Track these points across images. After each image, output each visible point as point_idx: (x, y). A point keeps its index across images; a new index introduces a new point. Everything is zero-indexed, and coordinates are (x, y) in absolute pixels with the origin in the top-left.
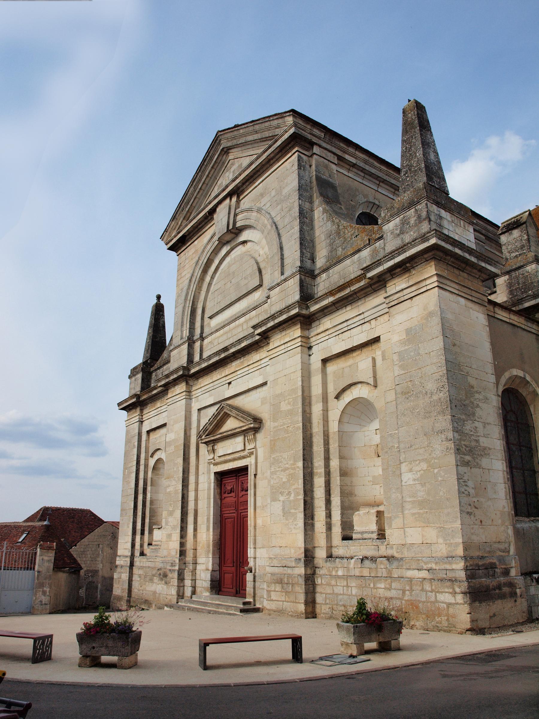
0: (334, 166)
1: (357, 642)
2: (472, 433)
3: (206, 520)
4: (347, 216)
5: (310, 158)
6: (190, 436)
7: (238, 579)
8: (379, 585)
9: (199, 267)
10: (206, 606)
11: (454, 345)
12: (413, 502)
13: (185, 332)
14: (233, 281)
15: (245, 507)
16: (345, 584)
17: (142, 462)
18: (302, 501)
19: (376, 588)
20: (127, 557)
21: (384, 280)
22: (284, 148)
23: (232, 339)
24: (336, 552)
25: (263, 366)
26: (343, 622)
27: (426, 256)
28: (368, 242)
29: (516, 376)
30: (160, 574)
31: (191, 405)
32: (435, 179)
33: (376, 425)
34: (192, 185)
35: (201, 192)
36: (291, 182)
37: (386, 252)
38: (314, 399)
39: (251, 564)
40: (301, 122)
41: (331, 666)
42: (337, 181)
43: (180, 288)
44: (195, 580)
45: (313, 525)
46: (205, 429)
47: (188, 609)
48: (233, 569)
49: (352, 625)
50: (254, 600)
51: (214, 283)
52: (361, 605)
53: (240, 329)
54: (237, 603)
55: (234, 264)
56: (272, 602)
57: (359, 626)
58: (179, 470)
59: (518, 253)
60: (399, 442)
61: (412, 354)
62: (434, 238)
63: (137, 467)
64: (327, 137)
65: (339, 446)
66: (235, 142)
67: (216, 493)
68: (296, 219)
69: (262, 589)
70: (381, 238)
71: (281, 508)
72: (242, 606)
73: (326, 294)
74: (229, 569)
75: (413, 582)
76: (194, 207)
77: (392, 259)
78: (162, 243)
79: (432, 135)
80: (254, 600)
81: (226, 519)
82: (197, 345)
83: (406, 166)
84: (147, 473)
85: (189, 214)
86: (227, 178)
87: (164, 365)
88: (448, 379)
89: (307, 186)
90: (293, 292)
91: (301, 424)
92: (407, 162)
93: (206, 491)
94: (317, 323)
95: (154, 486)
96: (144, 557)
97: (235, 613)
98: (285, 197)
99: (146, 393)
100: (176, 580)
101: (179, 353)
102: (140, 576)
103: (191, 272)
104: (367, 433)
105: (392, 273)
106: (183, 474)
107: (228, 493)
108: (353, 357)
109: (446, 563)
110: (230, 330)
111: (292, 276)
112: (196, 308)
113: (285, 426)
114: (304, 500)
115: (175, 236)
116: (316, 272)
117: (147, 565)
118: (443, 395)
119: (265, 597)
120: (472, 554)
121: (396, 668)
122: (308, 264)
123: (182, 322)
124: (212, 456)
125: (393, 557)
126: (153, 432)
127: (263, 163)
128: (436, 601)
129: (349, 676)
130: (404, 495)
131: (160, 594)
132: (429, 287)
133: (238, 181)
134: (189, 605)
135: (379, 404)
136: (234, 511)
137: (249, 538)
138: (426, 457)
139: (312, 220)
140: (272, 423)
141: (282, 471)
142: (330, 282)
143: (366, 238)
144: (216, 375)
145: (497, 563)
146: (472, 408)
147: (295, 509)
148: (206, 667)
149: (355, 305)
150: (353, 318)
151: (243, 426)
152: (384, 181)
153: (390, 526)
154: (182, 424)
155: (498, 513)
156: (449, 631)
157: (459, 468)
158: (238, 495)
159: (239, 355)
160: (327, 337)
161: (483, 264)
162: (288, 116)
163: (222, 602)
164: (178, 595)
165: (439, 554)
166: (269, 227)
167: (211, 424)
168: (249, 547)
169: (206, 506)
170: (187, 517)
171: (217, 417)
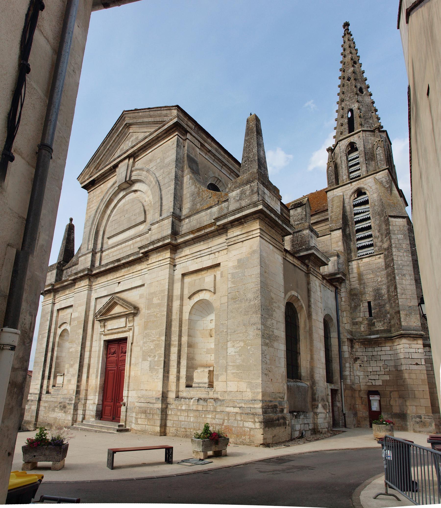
0: (198, 149)
1: (204, 451)
2: (270, 326)
3: (95, 372)
4: (204, 184)
5: (184, 141)
6: (89, 315)
7: (115, 410)
8: (208, 416)
9: (103, 203)
10: (93, 427)
11: (265, 272)
12: (233, 366)
13: (90, 245)
14: (126, 216)
15: (123, 364)
16: (187, 414)
17: (53, 330)
18: (163, 362)
19: (206, 418)
20: (36, 394)
21: (226, 228)
22: (168, 131)
23: (122, 254)
24: (181, 394)
25: (143, 274)
26: (196, 438)
27: (254, 216)
28: (217, 202)
29: (294, 295)
30: (61, 406)
31: (91, 294)
32: (262, 168)
33: (212, 316)
34: (102, 145)
35: (108, 151)
36: (171, 155)
37: (230, 210)
38: (175, 298)
39: (125, 400)
40: (181, 115)
41: (191, 466)
42: (199, 159)
43: (89, 215)
44: (85, 410)
45: (168, 377)
46: (100, 312)
47: (80, 430)
48: (112, 403)
49: (202, 440)
50: (126, 424)
51: (112, 216)
52: (207, 428)
53: (128, 248)
54: (114, 426)
55: (127, 204)
56: (138, 425)
57: (206, 441)
58: (79, 338)
59: (299, 222)
60: (227, 329)
61: (240, 275)
62: (262, 205)
63: (48, 334)
64: (196, 129)
65: (188, 329)
66: (135, 121)
67: (104, 354)
68: (172, 180)
69: (131, 416)
70: (227, 200)
71: (149, 365)
72: (118, 428)
73: (189, 232)
74: (109, 403)
75: (230, 415)
76: (103, 161)
77: (233, 215)
78: (78, 183)
79: (263, 140)
80: (126, 424)
81: (109, 371)
82: (98, 255)
83: (246, 157)
84: (55, 338)
85: (98, 166)
86: (127, 145)
87: (73, 266)
88: (261, 292)
89: (181, 159)
90: (167, 228)
91: (166, 313)
92: (247, 154)
93: (97, 352)
94: (181, 250)
95: (59, 347)
96: (49, 394)
97: (113, 432)
98: (167, 164)
99: (59, 284)
100: (72, 410)
101: (85, 259)
102: (45, 407)
103: (98, 205)
104: (205, 322)
105: (232, 224)
106: (82, 340)
107: (112, 354)
108: (202, 274)
109: (251, 404)
110: (121, 248)
111: (167, 218)
112: (99, 230)
113: (155, 313)
114: (164, 361)
115: (88, 179)
116: (182, 218)
117: (51, 400)
118: (257, 302)
119: (134, 422)
120: (266, 399)
121: (229, 467)
122: (178, 211)
123: (89, 239)
124: (103, 330)
125: (218, 399)
126: (62, 310)
127: (154, 139)
128: (243, 427)
129: (205, 472)
130: (228, 361)
131: (59, 419)
132: (254, 236)
133: (135, 148)
134: (81, 426)
135: (216, 304)
136: (115, 366)
137: (124, 384)
138: (243, 339)
139: (182, 183)
140: (146, 311)
141: (151, 341)
142: (190, 225)
143: (216, 200)
144: (110, 277)
145: (278, 405)
146: (271, 311)
147: (158, 366)
148: (113, 468)
149: (206, 242)
150: (204, 250)
151: (126, 311)
152: (225, 165)
153: (217, 380)
154: (84, 307)
155: (280, 375)
156: (250, 445)
157: (263, 346)
158: (119, 356)
159: (127, 265)
160: (186, 260)
161: (285, 226)
162: (174, 109)
163: (104, 425)
164: (73, 420)
165: (247, 398)
166: (154, 183)
167: (104, 308)
168: (124, 389)
169: (96, 362)
170: (82, 369)
171: (109, 304)
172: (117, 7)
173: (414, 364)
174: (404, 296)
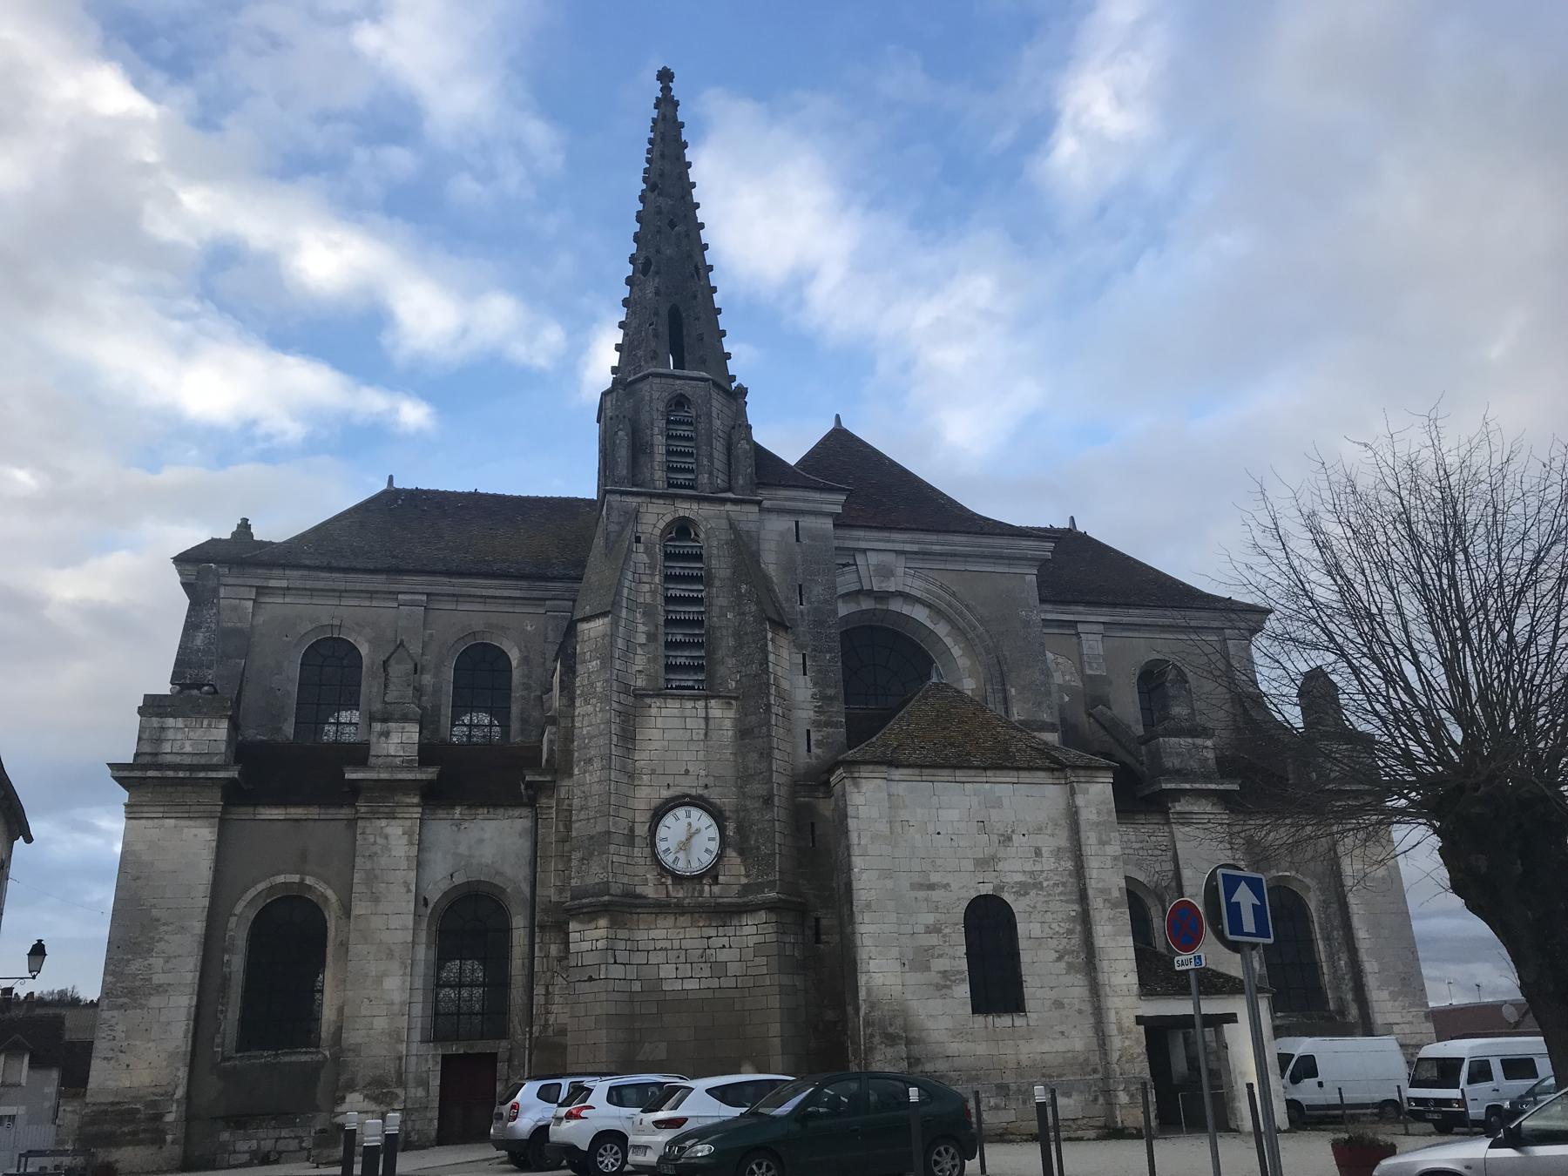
128: (1372, 546)
172: (748, 409)
173: (586, 979)
174: (583, 815)
